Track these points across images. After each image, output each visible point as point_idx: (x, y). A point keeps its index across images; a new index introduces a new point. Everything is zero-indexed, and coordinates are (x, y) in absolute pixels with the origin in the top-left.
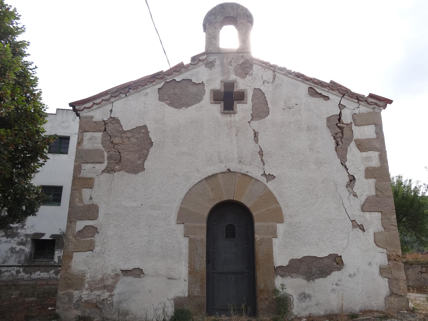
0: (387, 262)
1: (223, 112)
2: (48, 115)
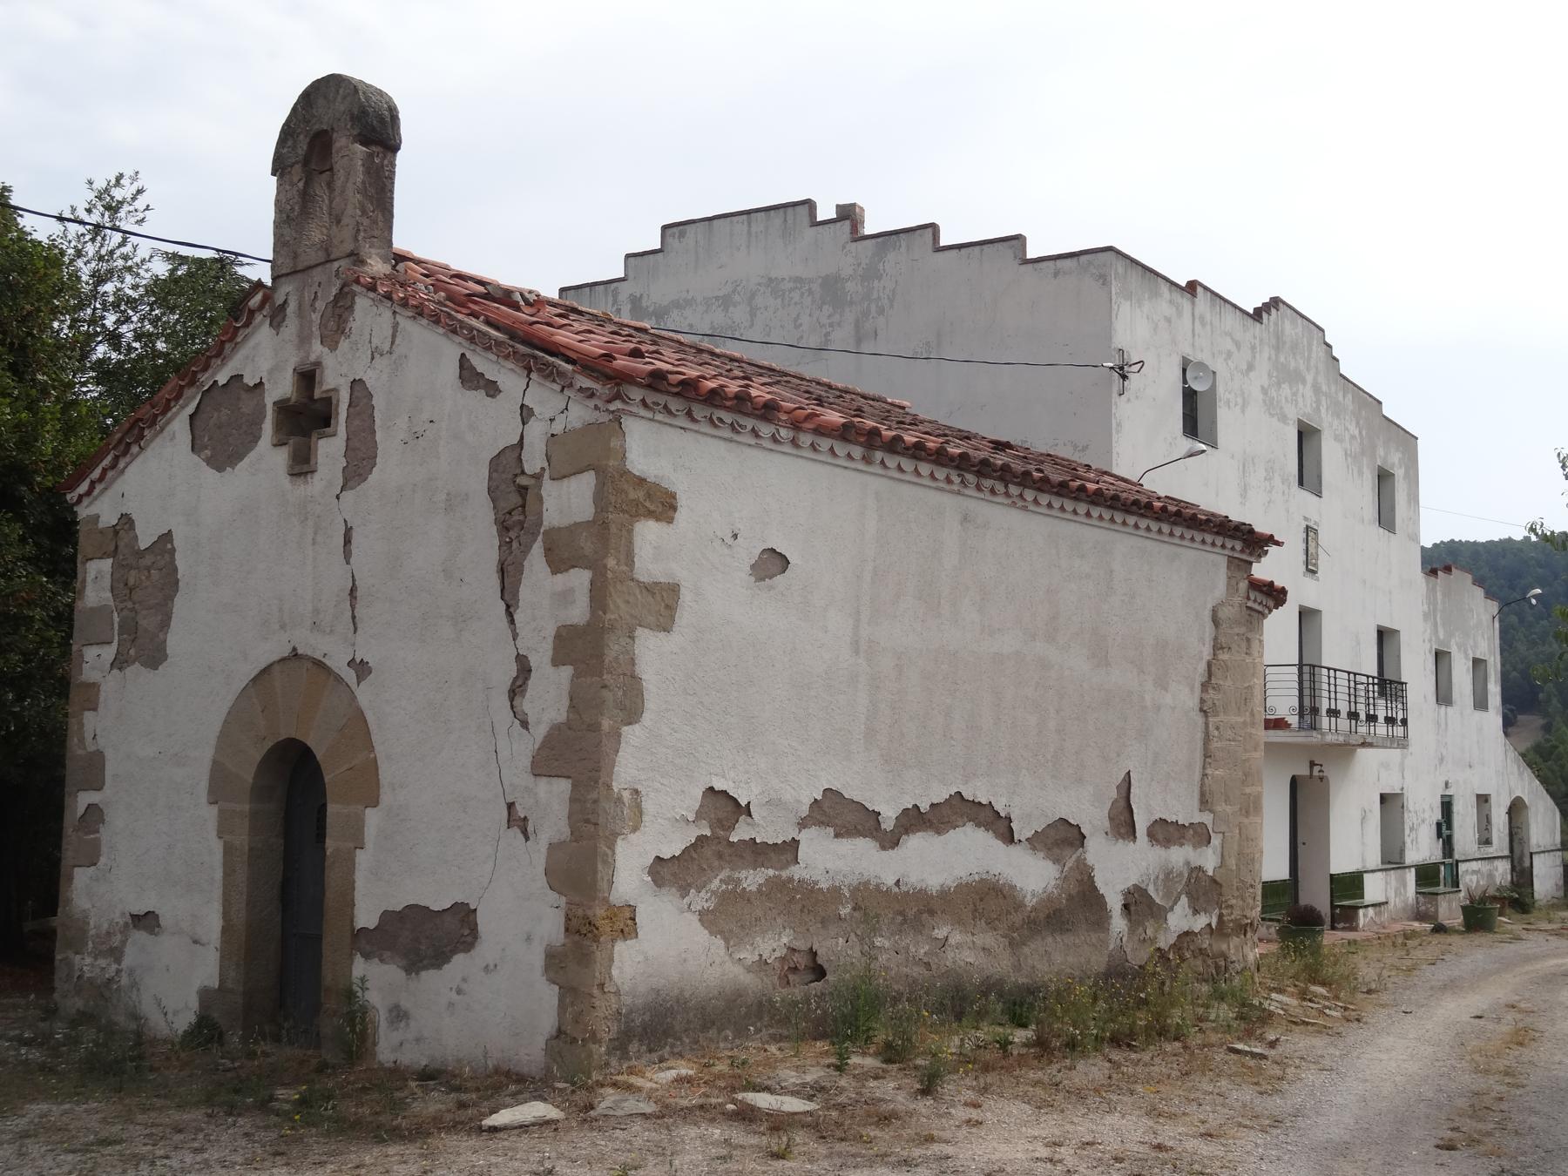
2: (1281, 305)
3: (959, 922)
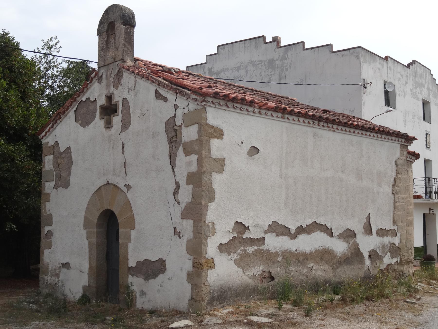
0: (192, 268)
1: (107, 127)
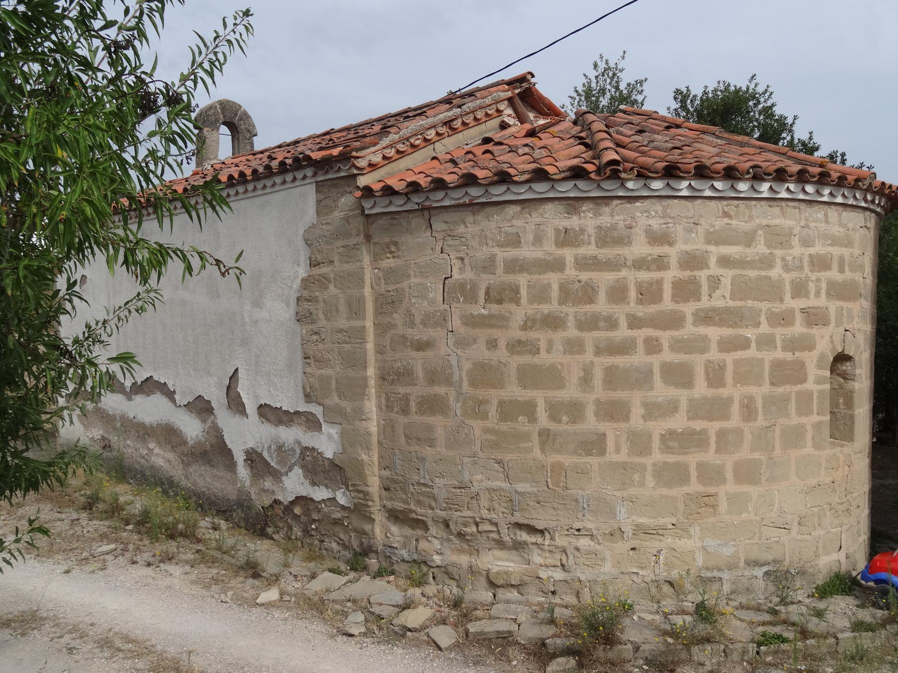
3: (159, 443)
